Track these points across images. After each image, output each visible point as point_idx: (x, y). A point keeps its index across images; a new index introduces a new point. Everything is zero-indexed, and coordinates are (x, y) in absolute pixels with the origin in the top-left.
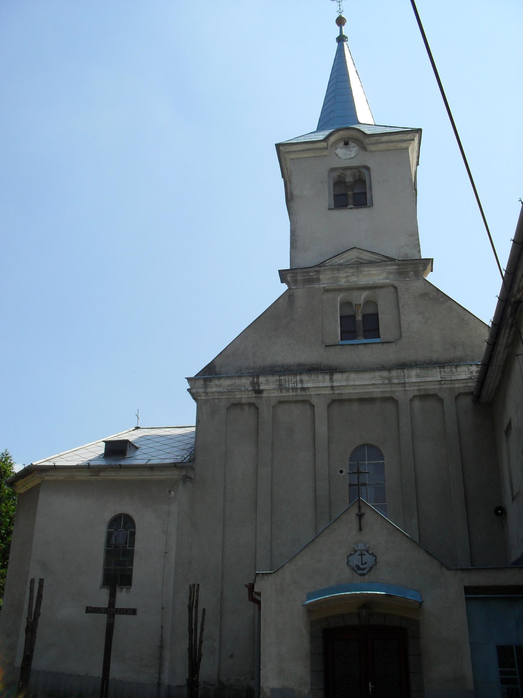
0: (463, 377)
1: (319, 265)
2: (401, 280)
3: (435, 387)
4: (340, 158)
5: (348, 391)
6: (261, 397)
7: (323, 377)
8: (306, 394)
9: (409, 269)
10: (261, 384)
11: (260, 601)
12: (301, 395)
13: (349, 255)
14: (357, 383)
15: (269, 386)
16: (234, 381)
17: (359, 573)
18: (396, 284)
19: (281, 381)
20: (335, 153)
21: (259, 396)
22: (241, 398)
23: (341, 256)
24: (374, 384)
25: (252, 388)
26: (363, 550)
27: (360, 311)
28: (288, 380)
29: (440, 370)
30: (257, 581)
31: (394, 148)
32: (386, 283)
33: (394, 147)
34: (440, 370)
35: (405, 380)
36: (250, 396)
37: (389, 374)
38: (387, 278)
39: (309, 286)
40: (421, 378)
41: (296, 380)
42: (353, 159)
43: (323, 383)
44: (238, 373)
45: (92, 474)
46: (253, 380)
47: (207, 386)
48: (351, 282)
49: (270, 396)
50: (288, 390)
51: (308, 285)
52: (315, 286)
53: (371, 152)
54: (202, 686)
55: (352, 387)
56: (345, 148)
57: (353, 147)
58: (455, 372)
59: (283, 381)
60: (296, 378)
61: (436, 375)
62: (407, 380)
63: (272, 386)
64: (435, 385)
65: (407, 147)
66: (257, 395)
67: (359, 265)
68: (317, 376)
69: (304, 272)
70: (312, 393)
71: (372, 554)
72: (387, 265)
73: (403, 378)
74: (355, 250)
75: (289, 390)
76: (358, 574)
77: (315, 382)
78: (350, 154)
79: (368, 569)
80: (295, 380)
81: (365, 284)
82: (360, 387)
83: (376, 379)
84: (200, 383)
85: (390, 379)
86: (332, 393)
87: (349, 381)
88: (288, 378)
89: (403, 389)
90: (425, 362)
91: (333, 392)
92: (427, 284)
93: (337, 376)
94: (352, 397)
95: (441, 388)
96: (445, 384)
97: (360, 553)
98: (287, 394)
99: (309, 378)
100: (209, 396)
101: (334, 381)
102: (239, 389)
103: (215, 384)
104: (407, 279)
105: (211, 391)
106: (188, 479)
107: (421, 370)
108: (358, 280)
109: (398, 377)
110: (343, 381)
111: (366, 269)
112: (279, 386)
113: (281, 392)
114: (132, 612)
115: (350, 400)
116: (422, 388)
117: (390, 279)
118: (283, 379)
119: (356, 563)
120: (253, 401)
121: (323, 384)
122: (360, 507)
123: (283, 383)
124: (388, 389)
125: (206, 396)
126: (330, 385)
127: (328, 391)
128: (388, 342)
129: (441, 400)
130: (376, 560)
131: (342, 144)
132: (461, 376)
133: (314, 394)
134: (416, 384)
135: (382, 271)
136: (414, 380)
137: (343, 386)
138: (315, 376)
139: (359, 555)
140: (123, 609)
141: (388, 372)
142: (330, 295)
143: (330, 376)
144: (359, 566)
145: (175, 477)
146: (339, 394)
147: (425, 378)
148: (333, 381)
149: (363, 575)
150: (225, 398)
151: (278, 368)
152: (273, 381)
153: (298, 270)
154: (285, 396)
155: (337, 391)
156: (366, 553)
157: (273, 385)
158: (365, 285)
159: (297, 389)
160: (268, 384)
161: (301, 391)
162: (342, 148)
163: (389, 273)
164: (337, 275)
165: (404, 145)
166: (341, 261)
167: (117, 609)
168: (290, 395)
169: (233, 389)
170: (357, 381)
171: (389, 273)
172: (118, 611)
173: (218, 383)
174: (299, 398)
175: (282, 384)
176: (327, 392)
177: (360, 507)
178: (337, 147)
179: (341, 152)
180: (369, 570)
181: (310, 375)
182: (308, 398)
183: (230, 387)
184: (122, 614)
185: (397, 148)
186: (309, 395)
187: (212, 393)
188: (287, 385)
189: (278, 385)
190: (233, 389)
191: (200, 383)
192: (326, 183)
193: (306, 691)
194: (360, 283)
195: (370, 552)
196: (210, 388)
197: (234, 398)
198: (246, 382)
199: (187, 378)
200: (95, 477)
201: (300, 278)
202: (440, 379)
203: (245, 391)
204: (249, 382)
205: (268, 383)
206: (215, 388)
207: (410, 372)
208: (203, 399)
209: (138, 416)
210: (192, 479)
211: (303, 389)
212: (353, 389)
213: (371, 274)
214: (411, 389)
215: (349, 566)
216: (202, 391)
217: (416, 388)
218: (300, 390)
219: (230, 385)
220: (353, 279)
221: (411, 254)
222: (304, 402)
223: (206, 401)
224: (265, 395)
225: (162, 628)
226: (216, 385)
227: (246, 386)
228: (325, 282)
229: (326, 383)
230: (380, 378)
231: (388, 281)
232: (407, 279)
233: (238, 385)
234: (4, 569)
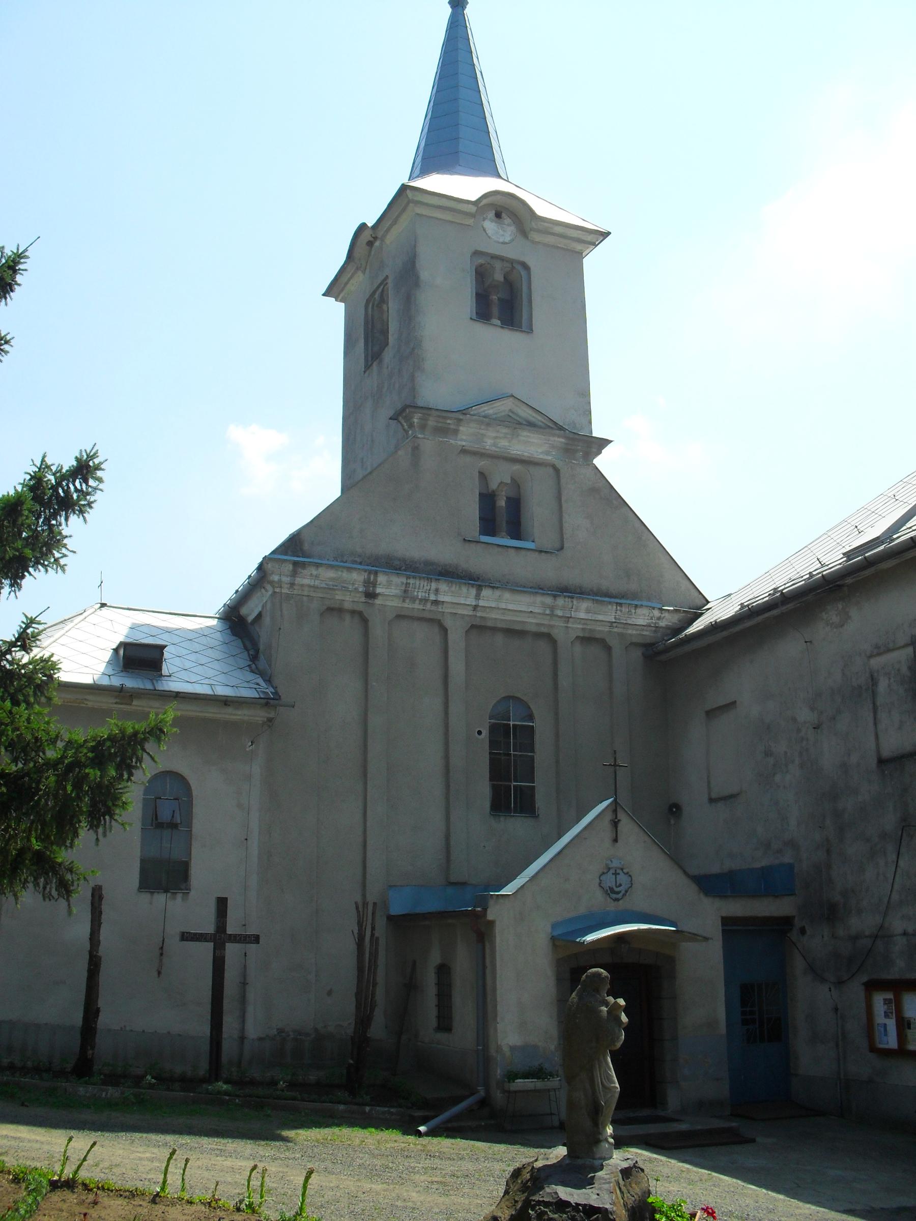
0: (641, 622)
1: (463, 412)
2: (566, 461)
4: (489, 237)
5: (494, 615)
6: (372, 603)
7: (468, 590)
9: (580, 448)
10: (379, 585)
12: (430, 611)
13: (503, 404)
14: (511, 607)
18: (559, 464)
19: (408, 586)
20: (483, 227)
23: (492, 404)
26: (619, 868)
27: (504, 493)
28: (419, 586)
29: (617, 608)
31: (564, 247)
32: (545, 459)
33: (565, 245)
34: (617, 608)
35: (571, 614)
36: (356, 600)
37: (553, 601)
38: (547, 453)
39: (441, 439)
40: (590, 614)
41: (430, 588)
42: (506, 245)
44: (338, 559)
45: (118, 701)
46: (369, 578)
47: (296, 574)
48: (499, 446)
49: (385, 605)
50: (413, 599)
51: (441, 438)
52: (451, 440)
53: (534, 242)
54: (292, 1036)
56: (496, 222)
57: (508, 225)
58: (633, 614)
59: (411, 585)
60: (431, 586)
61: (609, 614)
63: (394, 591)
65: (582, 250)
67: (517, 426)
69: (439, 416)
70: (447, 611)
71: (628, 873)
72: (554, 435)
74: (511, 399)
75: (415, 600)
77: (455, 596)
78: (503, 235)
79: (623, 892)
81: (518, 455)
86: (473, 614)
87: (500, 602)
88: (420, 584)
90: (591, 590)
91: (475, 614)
92: (599, 475)
93: (486, 592)
94: (499, 625)
95: (610, 631)
96: (616, 627)
97: (614, 872)
98: (410, 606)
100: (294, 589)
104: (573, 461)
105: (301, 583)
107: (593, 604)
108: (509, 446)
111: (525, 434)
113: (404, 601)
114: (254, 940)
115: (494, 629)
116: (588, 627)
117: (552, 454)
118: (413, 584)
120: (360, 607)
123: (410, 589)
124: (546, 622)
125: (289, 589)
126: (474, 604)
127: (468, 612)
128: (546, 552)
129: (608, 649)
131: (491, 214)
132: (639, 619)
133: (448, 612)
134: (583, 621)
135: (545, 442)
136: (582, 615)
138: (458, 587)
139: (613, 874)
140: (239, 935)
141: (552, 598)
142: (468, 459)
144: (613, 888)
145: (257, 718)
146: (481, 617)
147: (596, 616)
148: (480, 599)
149: (617, 900)
151: (397, 562)
153: (433, 412)
156: (620, 872)
157: (396, 589)
158: (518, 457)
160: (389, 587)
161: (432, 605)
162: (492, 221)
163: (553, 447)
164: (483, 432)
165: (579, 247)
166: (491, 412)
167: (230, 935)
168: (414, 608)
169: (336, 586)
171: (553, 447)
172: (232, 938)
173: (315, 572)
174: (427, 615)
175: (408, 590)
176: (465, 612)
178: (485, 216)
179: (490, 226)
181: (450, 584)
182: (439, 617)
184: (239, 943)
185: (569, 248)
187: (302, 585)
188: (416, 594)
190: (336, 586)
192: (468, 272)
193: (553, 1047)
194: (512, 452)
196: (300, 578)
198: (357, 578)
200: (122, 706)
201: (431, 422)
202: (614, 620)
205: (389, 586)
207: (580, 604)
209: (101, 585)
211: (436, 602)
213: (530, 442)
214: (574, 626)
216: (288, 581)
217: (580, 626)
218: (430, 603)
219: (332, 579)
220: (504, 443)
221: (579, 424)
222: (430, 621)
224: (378, 601)
225: (246, 956)
227: (355, 584)
228: (464, 437)
229: (469, 599)
230: (541, 606)
231: (550, 458)
232: (573, 461)
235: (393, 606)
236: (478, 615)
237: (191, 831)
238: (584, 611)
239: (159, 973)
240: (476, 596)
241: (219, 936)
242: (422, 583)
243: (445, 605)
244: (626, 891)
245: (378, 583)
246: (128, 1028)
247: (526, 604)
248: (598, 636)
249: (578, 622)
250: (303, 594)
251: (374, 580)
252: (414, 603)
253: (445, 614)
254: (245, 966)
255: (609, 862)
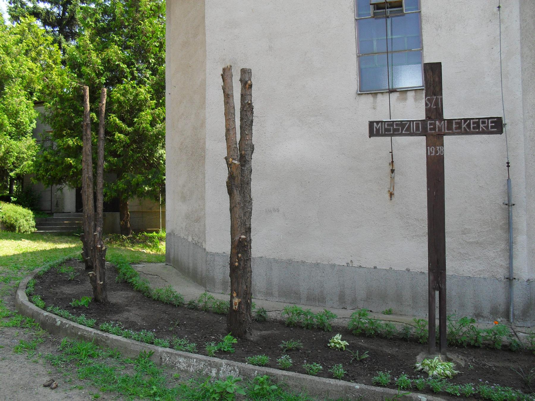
140: (466, 120)
167: (450, 121)
225: (508, 166)
234: (159, 108)
237: (420, 12)
239: (391, 195)
241: (431, 124)
246: (356, 264)
254: (509, 180)
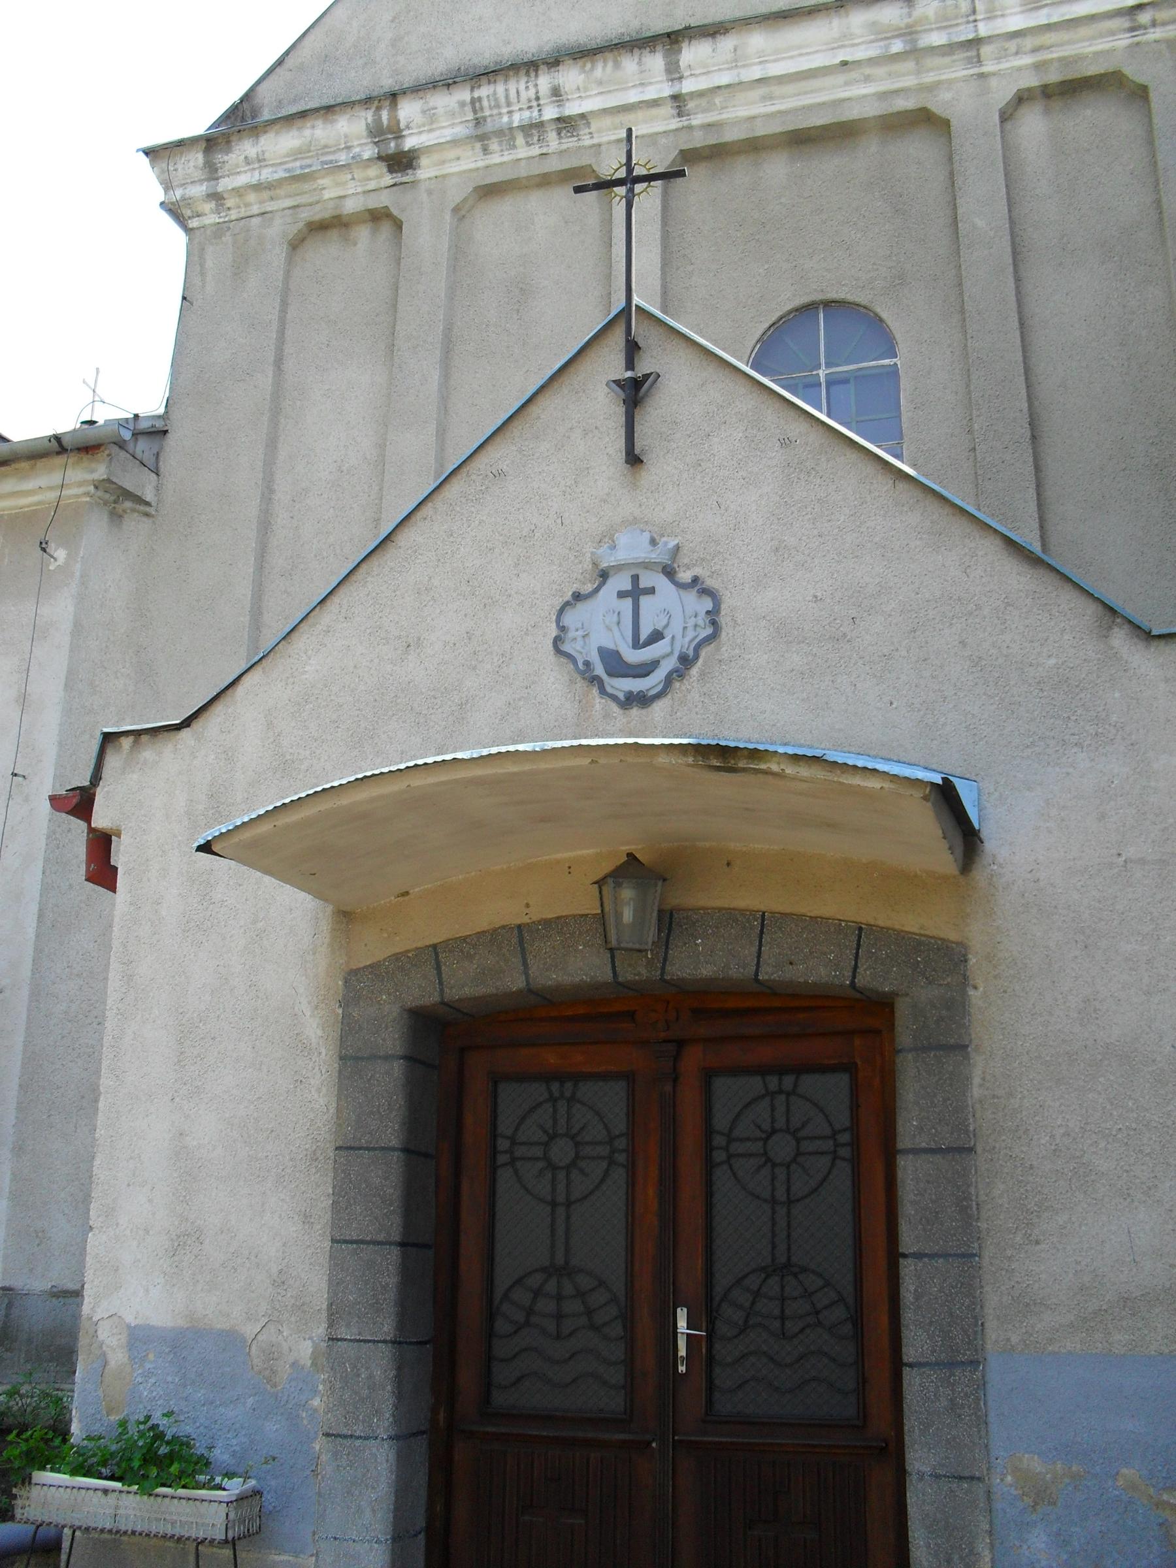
3: (1107, 46)
7: (640, 63)
8: (581, 143)
10: (408, 127)
11: (117, 868)
15: (437, 133)
16: (307, 132)
17: (621, 696)
19: (477, 105)
21: (405, 179)
22: (340, 197)
24: (844, 63)
25: (376, 151)
26: (647, 565)
28: (507, 97)
30: (107, 772)
35: (976, 31)
36: (372, 185)
37: (906, 10)
40: (1045, 11)
41: (537, 92)
43: (640, 89)
46: (378, 120)
47: (216, 170)
49: (444, 176)
50: (506, 135)
55: (762, 91)
59: (485, 103)
60: (536, 85)
62: (983, 30)
64: (1112, 33)
66: (399, 178)
68: (617, 65)
70: (605, 139)
71: (695, 580)
73: (968, 22)
75: (513, 138)
76: (614, 698)
80: (532, 92)
82: (789, 89)
83: (856, 41)
84: (192, 164)
85: (911, 33)
86: (680, 125)
87: (744, 66)
89: (971, 72)
91: (686, 123)
93: (693, 54)
94: (761, 130)
96: (1154, 24)
97: (627, 585)
98: (507, 157)
99: (583, 76)
100: (229, 209)
101: (686, 74)
102: (331, 162)
103: (242, 157)
106: (128, 504)
109: (947, 19)
110: (720, 70)
112: (475, 126)
113: (485, 150)
115: (754, 147)
116: (1055, 55)
118: (488, 96)
119: (603, 638)
121: (641, 92)
122: (632, 349)
123: (487, 113)
124: (909, 81)
130: (713, 618)
133: (609, 143)
134: (1028, 43)
137: (719, 87)
138: (610, 64)
139: (622, 595)
143: (665, 56)
146: (709, 126)
148: (681, 78)
150: (284, 209)
152: (448, 109)
154: (501, 164)
155: (699, 116)
159: (540, 125)
169: (310, 166)
170: (775, 61)
175: (484, 118)
176: (659, 127)
177: (632, 349)
180: (676, 670)
181: (589, 66)
182: (584, 161)
183: (296, 159)
186: (594, 145)
187: (237, 192)
189: (471, 125)
191: (192, 164)
195: (685, 576)
197: (317, 202)
199: (149, 152)
203: (349, 164)
204: (364, 127)
205: (432, 123)
206: (245, 172)
208: (211, 225)
210: (148, 504)
211: (566, 124)
212: (764, 98)
215: (563, 660)
217: (1027, 60)
219: (297, 154)
223: (219, 230)
224: (426, 171)
226: (247, 160)
233: (326, 146)
235: (465, 172)
236: (695, 122)
238: (1018, 9)
240: (668, 71)
242: (512, 86)
243: (595, 125)
244: (686, 661)
245: (402, 126)
247: (824, 47)
248: (1092, 70)
249: (1013, 49)
250: (249, 214)
251: (389, 120)
252: (514, 147)
253: (603, 148)
255: (603, 550)
